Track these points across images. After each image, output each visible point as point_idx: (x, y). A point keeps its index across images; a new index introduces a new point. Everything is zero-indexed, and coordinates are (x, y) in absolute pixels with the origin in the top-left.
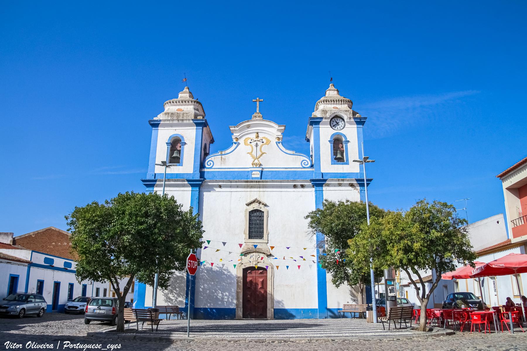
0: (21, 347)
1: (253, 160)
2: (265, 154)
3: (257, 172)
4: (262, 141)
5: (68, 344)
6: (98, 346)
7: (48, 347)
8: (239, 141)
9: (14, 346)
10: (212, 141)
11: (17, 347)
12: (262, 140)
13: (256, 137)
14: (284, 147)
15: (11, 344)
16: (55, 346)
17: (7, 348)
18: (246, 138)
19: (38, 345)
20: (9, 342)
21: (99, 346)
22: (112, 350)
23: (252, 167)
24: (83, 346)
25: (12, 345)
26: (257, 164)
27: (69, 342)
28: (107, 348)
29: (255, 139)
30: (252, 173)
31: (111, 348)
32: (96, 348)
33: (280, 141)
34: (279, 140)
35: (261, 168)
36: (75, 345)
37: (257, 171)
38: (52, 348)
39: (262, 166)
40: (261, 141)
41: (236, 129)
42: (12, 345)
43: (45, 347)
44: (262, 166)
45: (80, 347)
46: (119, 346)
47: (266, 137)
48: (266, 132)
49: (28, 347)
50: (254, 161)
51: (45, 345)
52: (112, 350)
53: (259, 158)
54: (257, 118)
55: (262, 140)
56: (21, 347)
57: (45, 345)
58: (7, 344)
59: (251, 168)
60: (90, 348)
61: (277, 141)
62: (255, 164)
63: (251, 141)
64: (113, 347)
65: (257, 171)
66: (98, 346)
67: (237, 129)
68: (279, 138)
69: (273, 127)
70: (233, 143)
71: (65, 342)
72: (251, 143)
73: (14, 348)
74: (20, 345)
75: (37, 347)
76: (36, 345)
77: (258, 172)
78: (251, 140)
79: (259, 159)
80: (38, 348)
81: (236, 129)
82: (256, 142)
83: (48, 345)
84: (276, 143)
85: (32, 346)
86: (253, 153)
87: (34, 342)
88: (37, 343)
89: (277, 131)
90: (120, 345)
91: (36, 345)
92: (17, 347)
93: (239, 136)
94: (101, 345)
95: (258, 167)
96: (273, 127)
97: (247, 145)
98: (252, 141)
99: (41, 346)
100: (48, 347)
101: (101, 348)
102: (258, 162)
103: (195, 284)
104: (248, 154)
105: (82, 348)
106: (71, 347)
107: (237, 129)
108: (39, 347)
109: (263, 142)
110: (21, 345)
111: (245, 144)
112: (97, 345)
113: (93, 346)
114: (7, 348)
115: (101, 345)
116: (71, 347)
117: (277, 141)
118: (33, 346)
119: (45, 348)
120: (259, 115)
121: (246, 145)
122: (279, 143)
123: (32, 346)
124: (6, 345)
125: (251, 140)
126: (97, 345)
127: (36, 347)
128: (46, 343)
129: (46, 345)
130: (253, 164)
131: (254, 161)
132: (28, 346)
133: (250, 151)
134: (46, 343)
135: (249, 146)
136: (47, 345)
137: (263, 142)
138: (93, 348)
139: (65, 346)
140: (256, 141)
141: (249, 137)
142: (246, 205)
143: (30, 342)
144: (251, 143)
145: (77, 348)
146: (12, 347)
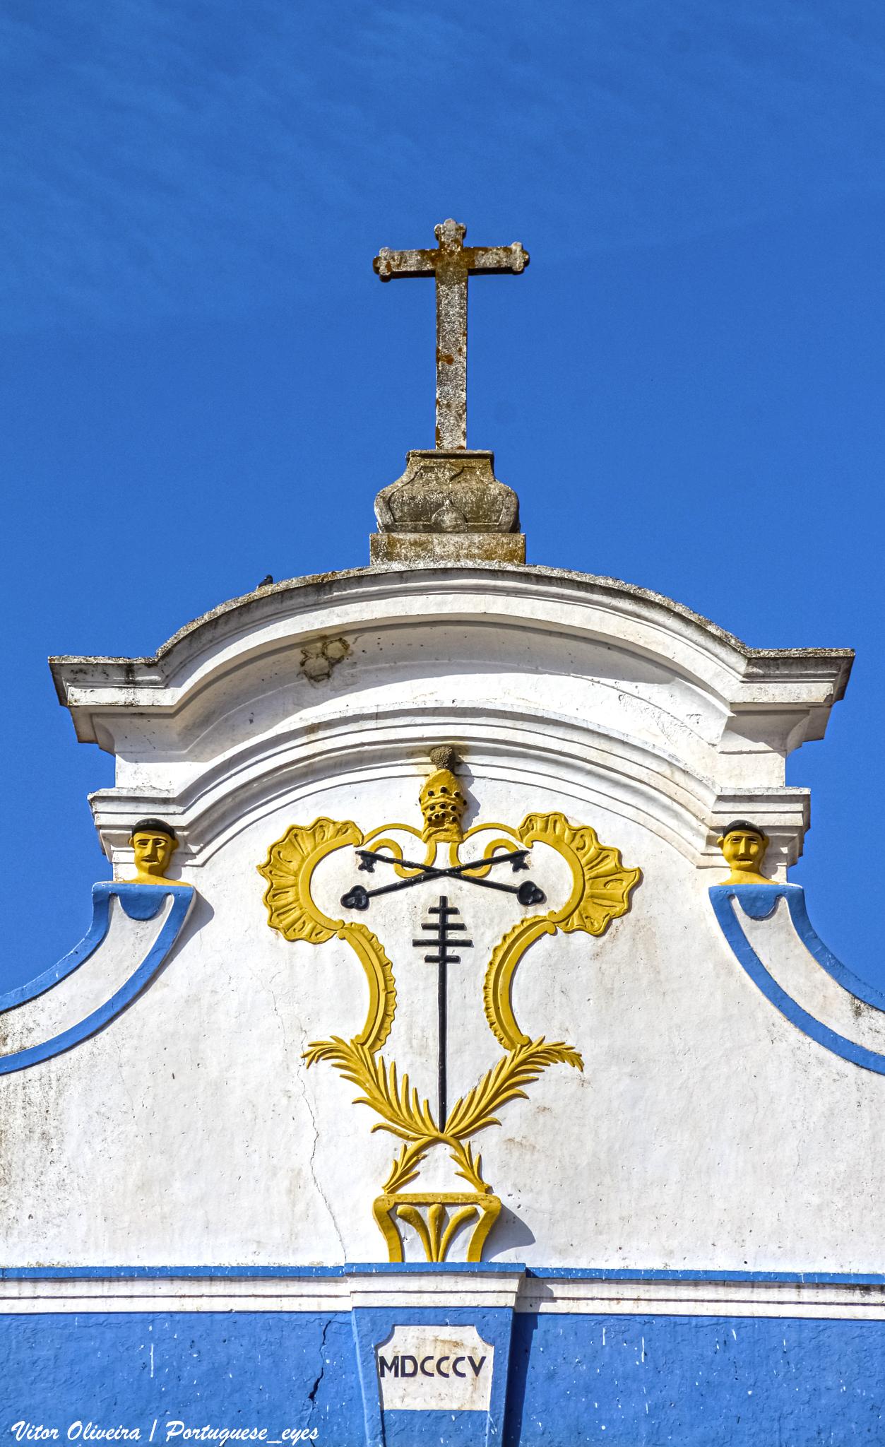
0: (55, 1437)
1: (390, 1148)
2: (561, 1069)
3: (447, 1333)
4: (517, 879)
5: (179, 1428)
6: (259, 1435)
7: (125, 1437)
8: (188, 876)
9: (36, 1434)
10: (801, 855)
11: (44, 1436)
12: (518, 860)
13: (435, 822)
14: (837, 969)
15: (30, 1428)
16: (145, 1433)
17: (18, 1439)
18: (293, 832)
19: (100, 1431)
20: (22, 1423)
21: (261, 1434)
22: (293, 1444)
23: (376, 1249)
24: (218, 1434)
25: (31, 1431)
26: (455, 1214)
27: (180, 1423)
28: (281, 1439)
29: (417, 852)
30: (387, 1352)
31: (292, 1438)
32: (253, 1438)
33: (780, 877)
34: (758, 864)
35: (504, 1272)
36: (198, 1431)
37: (458, 1316)
38: (137, 1438)
39: (525, 1237)
40: (503, 873)
41: (144, 697)
42: (31, 1431)
43: (118, 1435)
44: (525, 1237)
45: (210, 1437)
46: (313, 1435)
47: (579, 816)
48: (575, 746)
49: (72, 1436)
50: (405, 1174)
51: (118, 1431)
52: (293, 1444)
53: (482, 1120)
54: (448, 548)
55: (518, 860)
56: (55, 1437)
57: (118, 1431)
58: (18, 1428)
59: (363, 1271)
60: (237, 1438)
61: (727, 875)
62: (428, 1214)
63: (371, 881)
64: (296, 1436)
65: (458, 1316)
66: (259, 1435)
67: (169, 697)
68: (755, 833)
69: (669, 672)
70: (103, 903)
71: (169, 1424)
72: (357, 899)
73: (36, 1438)
74: (53, 1431)
75: (97, 1436)
76: (93, 1431)
77: (470, 1338)
78: (369, 861)
79: (485, 1143)
80: (99, 1438)
81: (144, 697)
82: (442, 886)
83: (127, 1431)
84: (721, 900)
85: (86, 1432)
86: (394, 1052)
87: (90, 1424)
88: (96, 1427)
89: (732, 727)
90: (316, 1431)
91: (93, 1431)
92: (44, 1436)
93: (187, 798)
94: (266, 1430)
95: (459, 1253)
96: (669, 672)
97: (315, 938)
98: (385, 874)
99: (108, 1434)
100: (125, 1437)
101: (265, 1440)
102: (466, 1188)
103: (482, 1277)
104: (325, 1065)
105: (215, 1438)
106: (186, 1436)
107: (169, 697)
108: (102, 1435)
109: (529, 894)
110: (56, 1431)
111: (277, 913)
112: (255, 1430)
113: (243, 1434)
114: (18, 1439)
115: (266, 1430)
116: (186, 1436)
117: (727, 875)
118: (87, 1435)
119: (117, 1438)
120: (466, 490)
121: (291, 933)
122: (761, 906)
123: (86, 1432)
124: (16, 1432)
125: (369, 861)
126: (255, 1430)
127: (94, 1435)
128: (121, 1427)
129: (121, 1430)
130: (387, 1218)
131: (405, 1174)
132: (73, 1434)
133: (352, 1028)
134: (121, 1427)
135: (334, 944)
136: (123, 1431)
137: (529, 894)
138: (244, 1438)
139: (171, 1434)
140: (430, 873)
141: (339, 816)
142: (485, 1357)
143: (78, 1423)
144: (357, 899)
145: (203, 1438)
146: (30, 1435)
